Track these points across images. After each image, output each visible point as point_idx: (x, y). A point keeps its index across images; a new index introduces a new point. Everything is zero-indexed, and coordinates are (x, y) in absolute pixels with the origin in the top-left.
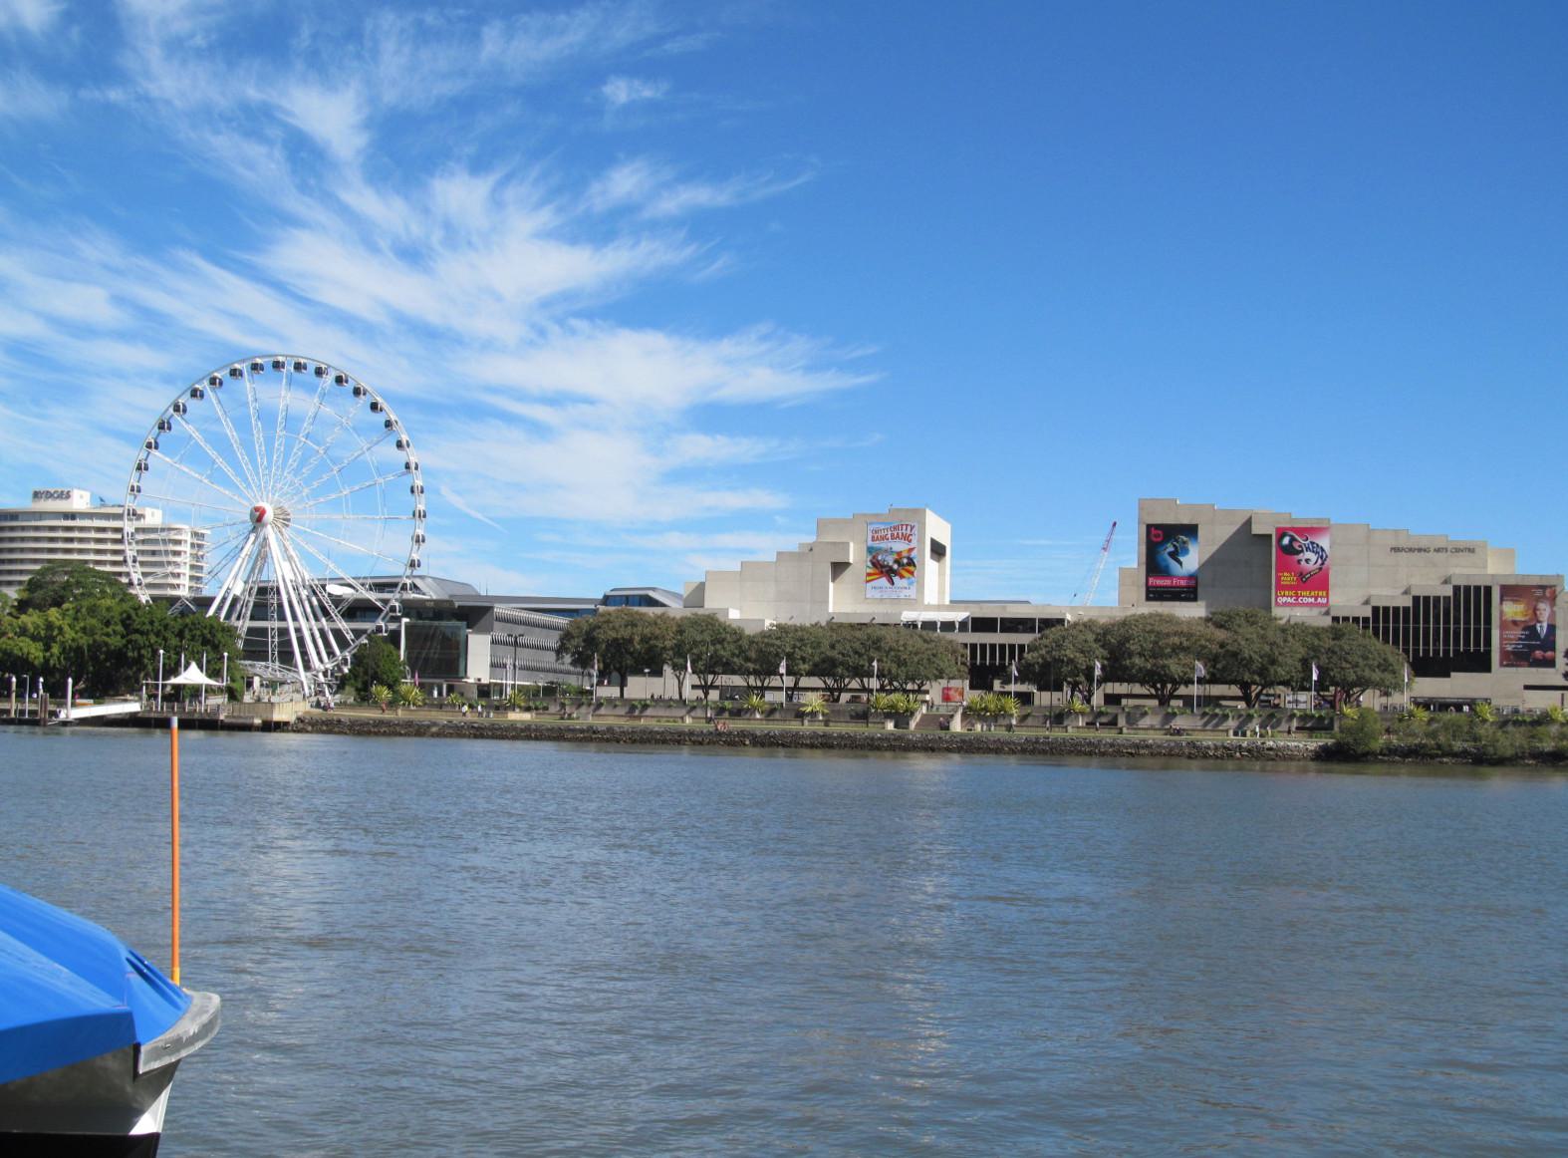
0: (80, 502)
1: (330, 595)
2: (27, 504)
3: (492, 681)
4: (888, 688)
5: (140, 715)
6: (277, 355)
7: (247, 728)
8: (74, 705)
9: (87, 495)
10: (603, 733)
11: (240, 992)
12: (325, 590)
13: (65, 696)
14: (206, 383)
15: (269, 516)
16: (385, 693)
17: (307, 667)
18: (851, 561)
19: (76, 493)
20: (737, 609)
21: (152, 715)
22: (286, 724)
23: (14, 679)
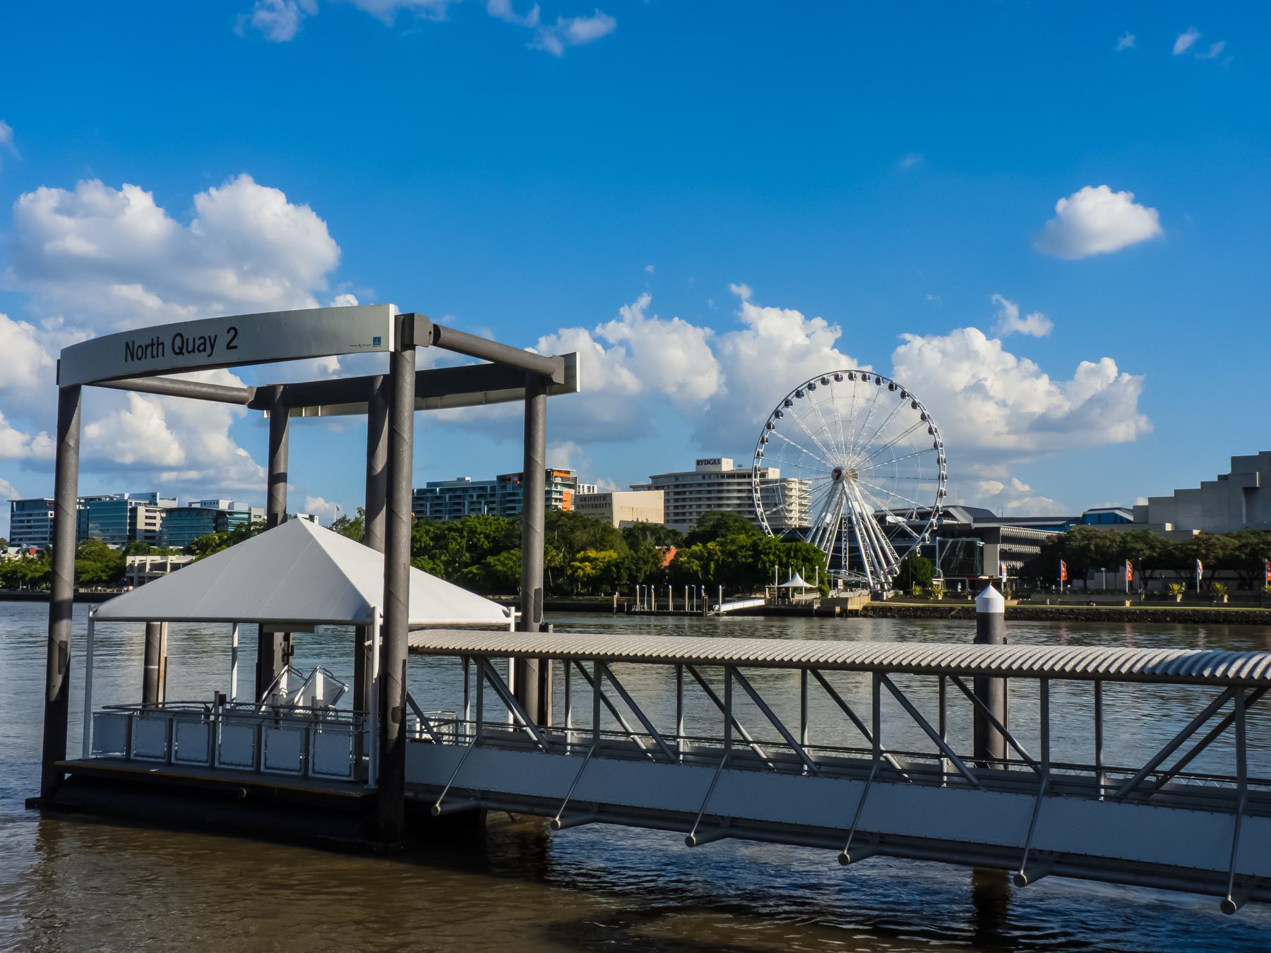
8: (724, 602)
10: (1066, 614)
16: (917, 590)
19: (724, 461)
21: (772, 607)
22: (857, 611)
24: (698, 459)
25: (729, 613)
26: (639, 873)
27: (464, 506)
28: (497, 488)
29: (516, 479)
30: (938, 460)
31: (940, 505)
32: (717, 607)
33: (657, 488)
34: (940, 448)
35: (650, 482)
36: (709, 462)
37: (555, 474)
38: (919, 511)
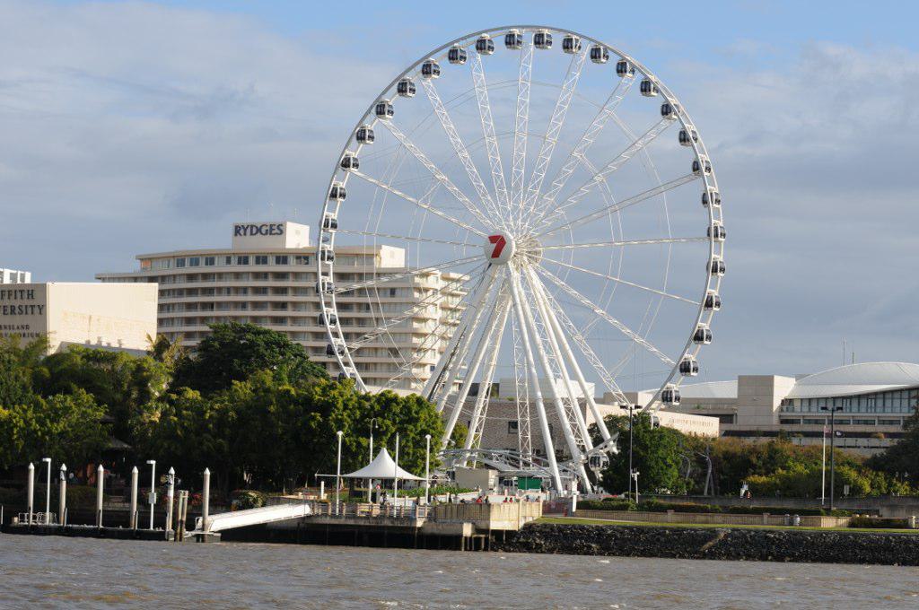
6: (481, 33)
7: (451, 542)
11: (12, 600)
14: (502, 39)
15: (514, 243)
19: (778, 380)
33: (152, 279)
35: (135, 267)
36: (259, 230)
38: (811, 506)
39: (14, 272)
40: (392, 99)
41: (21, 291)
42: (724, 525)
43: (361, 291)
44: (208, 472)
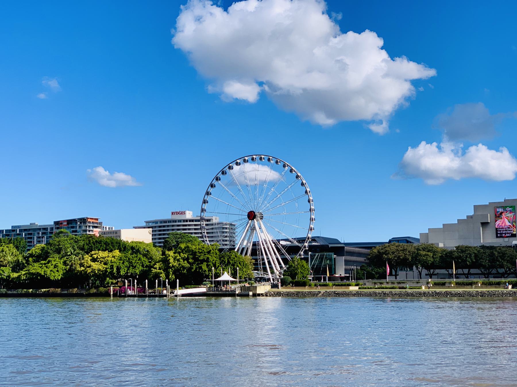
0: (189, 215)
1: (281, 245)
2: (169, 217)
3: (345, 275)
4: (509, 272)
5: (205, 293)
9: (191, 213)
12: (280, 244)
13: (176, 287)
17: (272, 272)
18: (489, 222)
19: (187, 212)
20: (442, 243)
23: (126, 281)
24: (173, 211)
25: (183, 295)
26: (109, 368)
27: (34, 239)
28: (54, 228)
29: (66, 223)
30: (310, 209)
31: (310, 236)
32: (176, 292)
33: (149, 228)
34: (311, 203)
35: (144, 224)
36: (179, 213)
37: (89, 220)
39: (109, 227)
40: (220, 175)
41: (114, 232)
42: (323, 290)
43: (212, 229)
44: (147, 281)
